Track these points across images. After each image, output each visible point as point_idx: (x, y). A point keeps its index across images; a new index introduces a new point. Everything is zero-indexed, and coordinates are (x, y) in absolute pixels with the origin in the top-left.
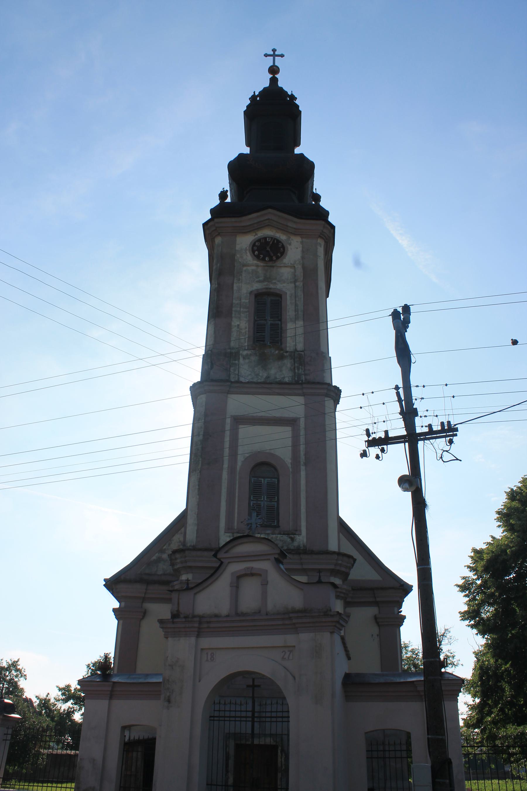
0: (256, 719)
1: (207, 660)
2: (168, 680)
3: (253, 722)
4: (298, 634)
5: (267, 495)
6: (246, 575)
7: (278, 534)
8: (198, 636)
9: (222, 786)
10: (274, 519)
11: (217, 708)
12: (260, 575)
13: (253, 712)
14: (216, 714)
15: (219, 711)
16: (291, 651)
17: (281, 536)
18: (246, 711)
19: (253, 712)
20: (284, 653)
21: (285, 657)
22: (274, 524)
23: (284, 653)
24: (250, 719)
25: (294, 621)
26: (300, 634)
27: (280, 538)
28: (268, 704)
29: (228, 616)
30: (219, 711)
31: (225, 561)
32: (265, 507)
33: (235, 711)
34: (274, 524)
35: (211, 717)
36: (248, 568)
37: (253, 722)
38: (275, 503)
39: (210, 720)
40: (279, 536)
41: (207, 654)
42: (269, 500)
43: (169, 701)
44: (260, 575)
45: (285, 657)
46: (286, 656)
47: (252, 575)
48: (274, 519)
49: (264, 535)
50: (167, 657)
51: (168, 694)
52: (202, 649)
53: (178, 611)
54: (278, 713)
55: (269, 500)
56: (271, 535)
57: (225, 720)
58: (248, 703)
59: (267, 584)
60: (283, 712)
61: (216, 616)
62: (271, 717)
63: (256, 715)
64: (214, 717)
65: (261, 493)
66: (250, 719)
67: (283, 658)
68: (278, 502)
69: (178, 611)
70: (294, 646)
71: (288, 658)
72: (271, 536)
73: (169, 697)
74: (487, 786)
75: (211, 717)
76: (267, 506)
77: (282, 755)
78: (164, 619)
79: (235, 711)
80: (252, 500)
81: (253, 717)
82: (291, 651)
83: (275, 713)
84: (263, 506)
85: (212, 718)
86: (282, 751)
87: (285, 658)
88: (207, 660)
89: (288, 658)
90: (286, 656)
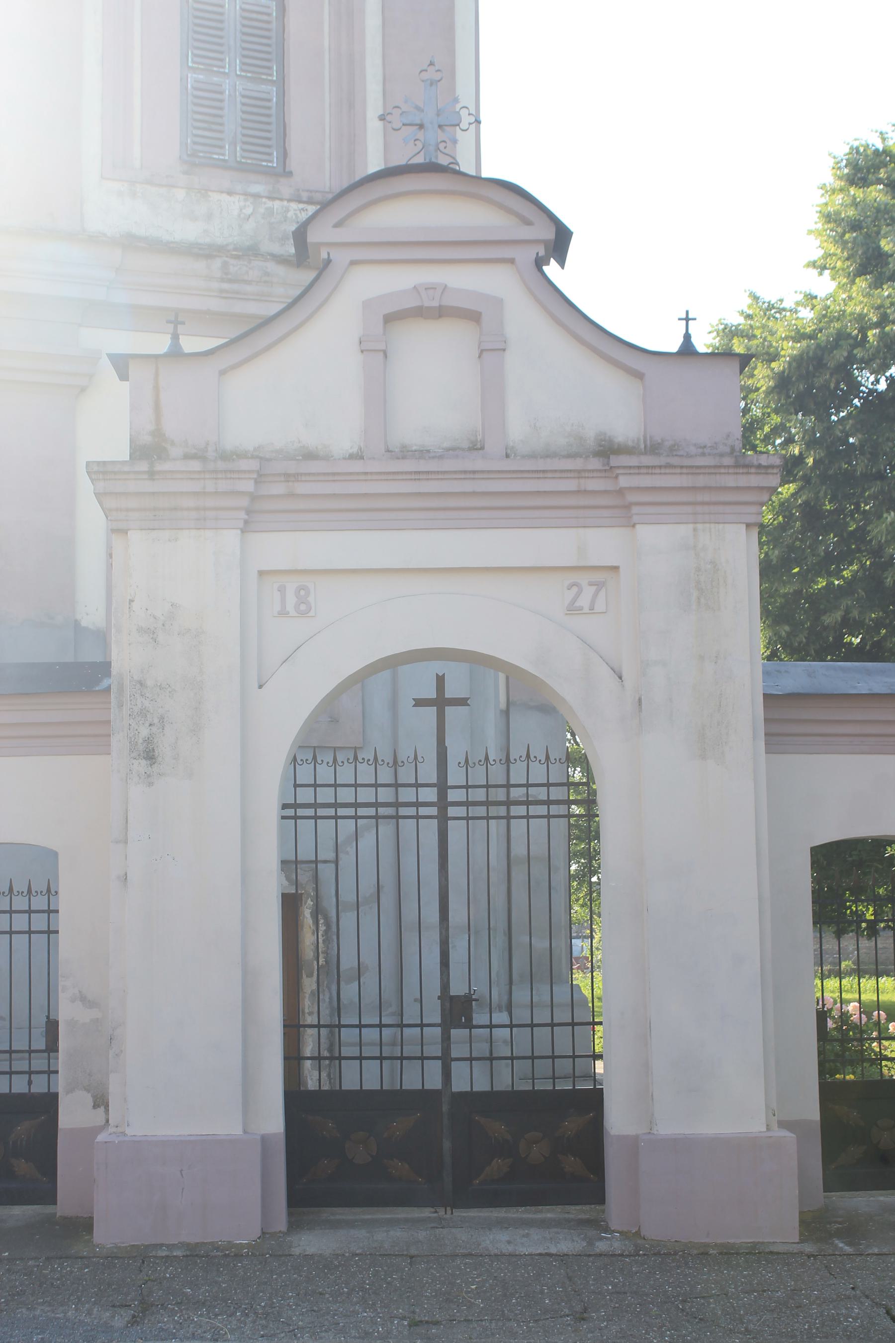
0: (452, 811)
1: (283, 613)
2: (141, 683)
3: (443, 820)
4: (634, 526)
5: (244, 56)
6: (420, 313)
7: (289, 200)
8: (245, 530)
9: (319, 1026)
10: (269, 147)
11: (305, 774)
12: (473, 317)
13: (442, 787)
14: (306, 795)
15: (356, 786)
16: (599, 586)
17: (301, 206)
18: (417, 785)
19: (442, 787)
20: (575, 589)
21: (577, 604)
22: (270, 164)
23: (575, 589)
24: (433, 811)
25: (624, 481)
26: (638, 526)
27: (296, 214)
28: (515, 760)
29: (358, 456)
30: (315, 786)
31: (340, 258)
32: (238, 99)
33: (376, 785)
34: (270, 164)
35: (285, 806)
36: (430, 288)
37: (443, 820)
38: (269, 87)
39: (283, 818)
40: (294, 206)
41: (282, 590)
42: (249, 75)
43: (150, 756)
44: (473, 317)
45: (577, 604)
46: (584, 601)
47: (441, 313)
48: (269, 147)
49: (242, 197)
50: (131, 601)
51: (144, 732)
52: (261, 573)
53: (158, 433)
54: (532, 790)
55: (249, 75)
56: (264, 200)
57: (397, 817)
58: (420, 759)
59: (504, 350)
60: (548, 785)
61: (310, 456)
62: (548, 803)
63: (453, 796)
64: (296, 806)
65: (221, 45)
66: (433, 811)
67: (573, 609)
68: (282, 84)
69: (158, 433)
70: (615, 569)
71: (592, 608)
72: (265, 203)
73: (148, 740)
74: (415, 1000)
75: (285, 806)
76: (244, 96)
77: (316, 923)
78: (113, 463)
79: (376, 785)
80: (192, 68)
81: (443, 803)
82: (599, 586)
83: (523, 790)
84: (230, 95)
85: (290, 812)
86: (317, 912)
87: (581, 608)
88: (283, 613)
89: (592, 608)
90: (584, 601)
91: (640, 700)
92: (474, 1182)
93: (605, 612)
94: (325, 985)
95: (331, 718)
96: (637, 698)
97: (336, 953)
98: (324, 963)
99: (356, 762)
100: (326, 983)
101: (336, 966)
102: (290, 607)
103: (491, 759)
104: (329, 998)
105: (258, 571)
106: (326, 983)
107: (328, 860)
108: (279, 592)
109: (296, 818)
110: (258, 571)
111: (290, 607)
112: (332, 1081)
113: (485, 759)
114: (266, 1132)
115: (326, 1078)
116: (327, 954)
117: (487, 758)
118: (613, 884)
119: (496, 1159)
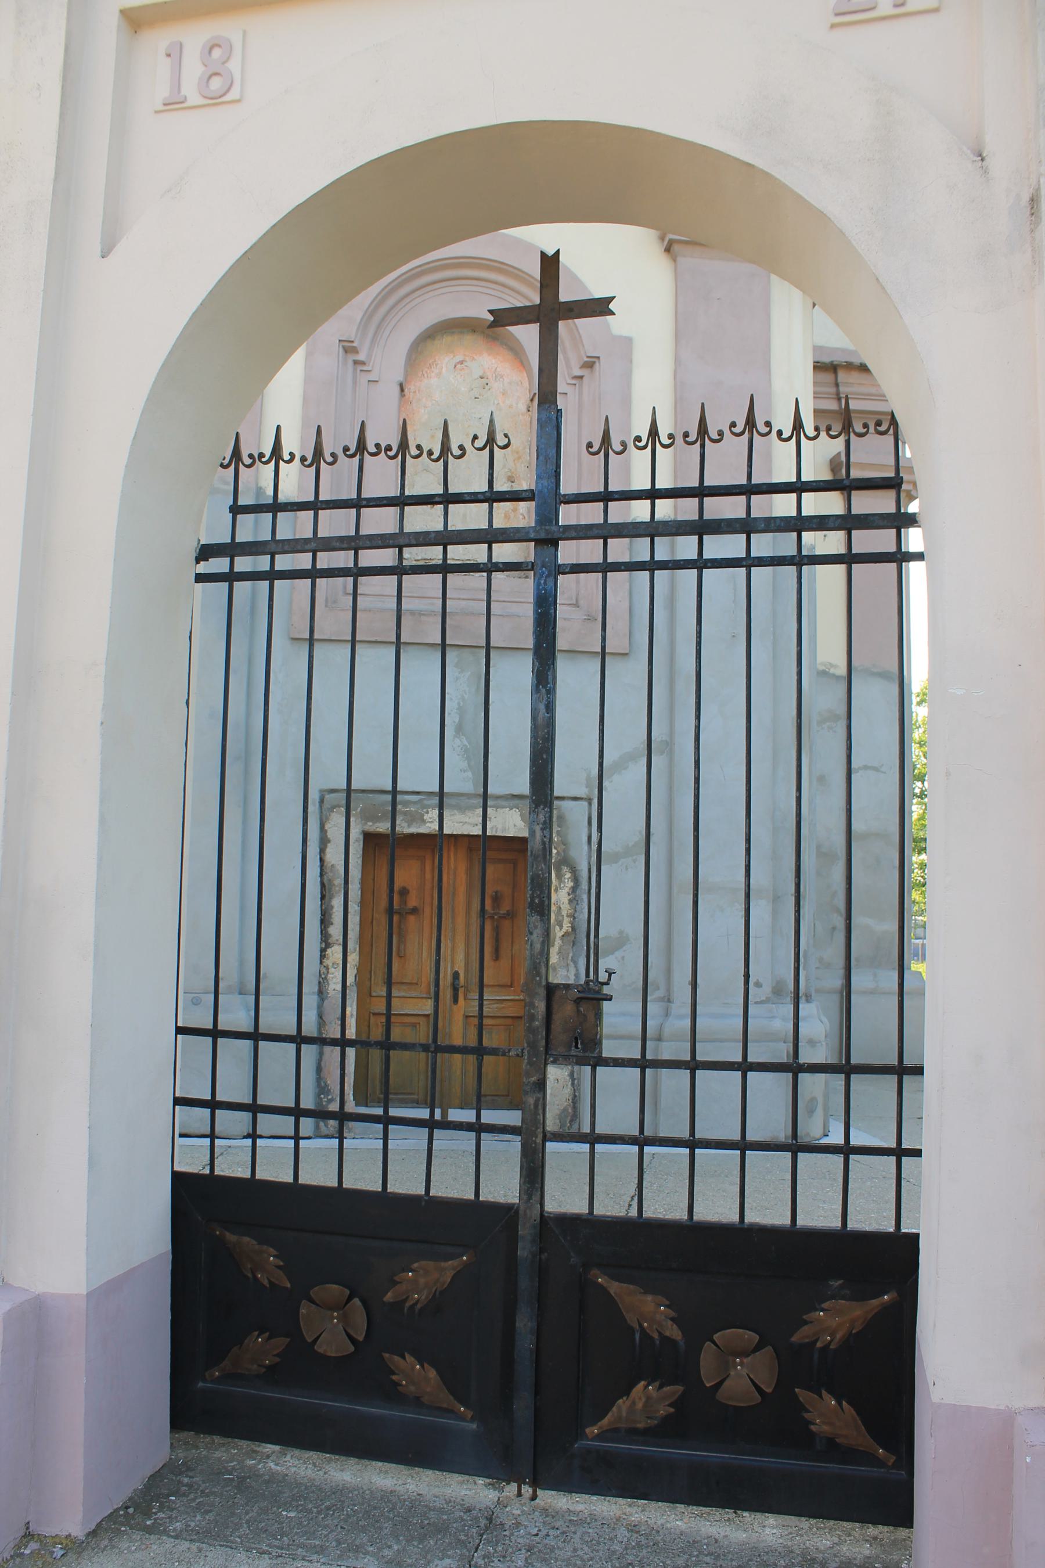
1: (174, 104)
35: (205, 552)
39: (200, 578)
41: (176, 53)
58: (501, 440)
85: (218, 565)
91: (1034, 201)
92: (588, 1430)
93: (936, 10)
94: (570, 958)
95: (589, 615)
96: (1026, 197)
97: (587, 916)
98: (570, 930)
99: (362, 455)
100: (571, 955)
101: (585, 934)
102: (191, 91)
103: (663, 433)
104: (575, 975)
105: (123, 12)
106: (571, 955)
107: (578, 796)
108: (169, 60)
109: (231, 577)
110: (123, 12)
111: (191, 91)
112: (576, 1081)
113: (650, 434)
114: (51, 1290)
115: (568, 1078)
116: (574, 918)
117: (654, 432)
118: (959, 692)
119: (643, 1383)
